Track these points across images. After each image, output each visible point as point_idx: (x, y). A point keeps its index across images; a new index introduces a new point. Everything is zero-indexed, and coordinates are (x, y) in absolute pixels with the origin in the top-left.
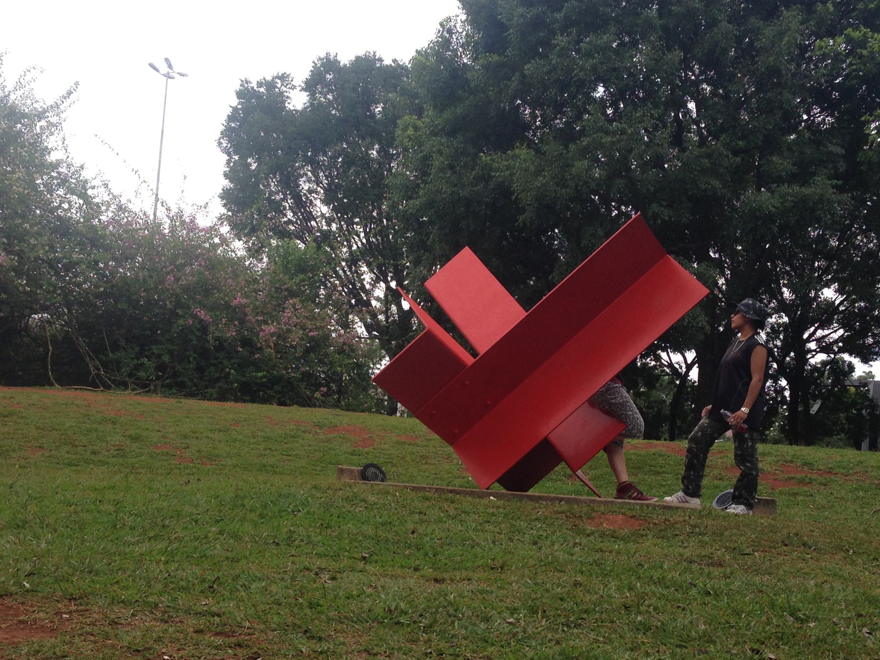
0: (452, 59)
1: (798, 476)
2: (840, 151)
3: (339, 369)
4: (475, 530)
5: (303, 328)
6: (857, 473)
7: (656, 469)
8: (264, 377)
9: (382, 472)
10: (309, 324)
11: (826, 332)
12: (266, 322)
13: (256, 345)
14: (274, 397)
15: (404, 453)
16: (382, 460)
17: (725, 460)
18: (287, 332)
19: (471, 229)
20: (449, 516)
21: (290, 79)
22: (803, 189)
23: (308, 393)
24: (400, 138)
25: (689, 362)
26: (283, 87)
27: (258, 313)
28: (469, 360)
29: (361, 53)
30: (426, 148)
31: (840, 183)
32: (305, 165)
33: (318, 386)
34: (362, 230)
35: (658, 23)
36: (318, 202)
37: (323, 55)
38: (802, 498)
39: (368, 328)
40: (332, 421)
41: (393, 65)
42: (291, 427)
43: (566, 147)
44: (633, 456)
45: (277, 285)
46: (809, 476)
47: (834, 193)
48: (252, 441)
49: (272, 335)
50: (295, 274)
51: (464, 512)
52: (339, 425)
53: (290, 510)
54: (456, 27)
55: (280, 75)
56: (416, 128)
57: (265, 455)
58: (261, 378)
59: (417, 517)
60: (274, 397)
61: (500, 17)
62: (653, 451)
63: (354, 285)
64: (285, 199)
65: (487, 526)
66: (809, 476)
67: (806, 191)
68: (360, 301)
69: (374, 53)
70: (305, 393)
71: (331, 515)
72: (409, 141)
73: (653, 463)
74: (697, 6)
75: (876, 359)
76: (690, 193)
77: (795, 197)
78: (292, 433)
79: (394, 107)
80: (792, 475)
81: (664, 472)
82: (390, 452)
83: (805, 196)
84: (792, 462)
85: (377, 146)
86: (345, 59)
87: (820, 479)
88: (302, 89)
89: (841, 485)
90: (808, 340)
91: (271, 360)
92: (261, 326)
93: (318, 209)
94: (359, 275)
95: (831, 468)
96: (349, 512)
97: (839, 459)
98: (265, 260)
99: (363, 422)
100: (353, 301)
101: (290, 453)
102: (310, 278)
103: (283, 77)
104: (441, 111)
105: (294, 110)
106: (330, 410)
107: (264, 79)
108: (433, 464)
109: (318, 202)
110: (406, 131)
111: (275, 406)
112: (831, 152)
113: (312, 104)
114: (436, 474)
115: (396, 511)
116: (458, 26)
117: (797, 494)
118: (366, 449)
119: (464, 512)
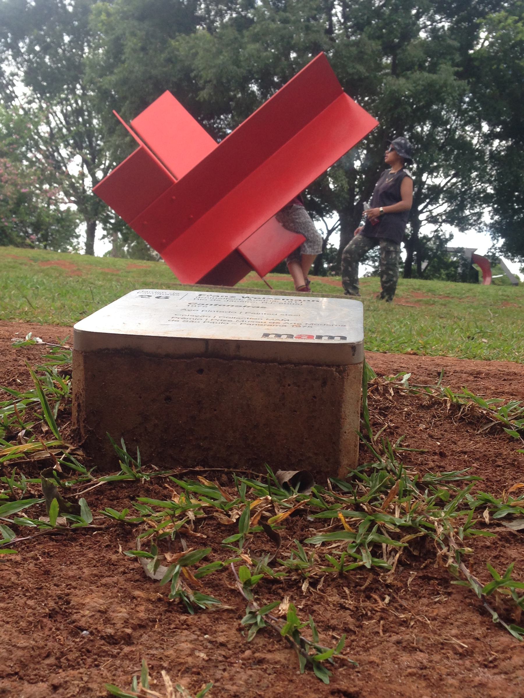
1: (425, 299)
5: (15, 185)
6: (468, 297)
10: (19, 181)
17: (368, 288)
22: (431, 75)
25: (330, 228)
28: (176, 181)
30: (118, 31)
31: (461, 69)
42: (9, 260)
46: (433, 299)
47: (455, 80)
56: (108, 15)
66: (433, 299)
67: (434, 77)
84: (419, 289)
87: (442, 301)
110: (99, 16)
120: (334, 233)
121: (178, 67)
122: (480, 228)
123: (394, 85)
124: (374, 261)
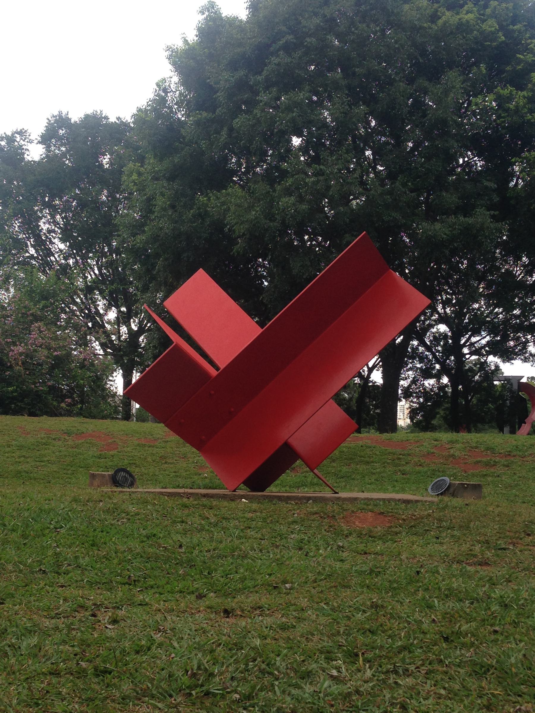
0: (168, 114)
1: (484, 459)
2: (493, 185)
3: (82, 382)
4: (239, 538)
5: (49, 348)
6: (531, 455)
7: (366, 459)
8: (16, 391)
9: (131, 475)
11: (478, 338)
12: (14, 343)
13: (6, 364)
14: (25, 408)
15: (145, 455)
16: (126, 462)
17: (421, 448)
18: (34, 352)
19: (191, 260)
20: (211, 523)
21: (28, 134)
22: (467, 219)
23: (55, 403)
24: (126, 183)
26: (22, 141)
27: (7, 336)
28: (214, 373)
29: (89, 112)
30: (149, 192)
31: (496, 213)
32: (44, 209)
33: (63, 397)
34: (95, 263)
35: (343, 83)
36: (56, 241)
37: (56, 113)
38: (491, 478)
39: (103, 346)
40: (79, 428)
41: (117, 122)
42: (43, 436)
43: (272, 186)
44: (344, 449)
45: (23, 311)
46: (493, 459)
47: (491, 222)
48: (8, 449)
49: (21, 354)
50: (39, 302)
51: (223, 518)
52: (85, 432)
53: (52, 526)
54: (170, 87)
55: (19, 130)
57: (20, 463)
58: (12, 392)
59: (179, 526)
60: (25, 408)
61: (209, 80)
62: (361, 443)
63: (89, 310)
64: (29, 238)
65: (250, 533)
66: (493, 459)
67: (470, 220)
68: (95, 324)
69: (101, 111)
70: (52, 404)
71: (95, 530)
72: (134, 185)
73: (362, 454)
74: (377, 68)
75: (516, 358)
76: (377, 225)
77: (461, 226)
78: (43, 441)
79: (120, 158)
80: (479, 459)
81: (373, 462)
82: (133, 454)
83: (469, 224)
85: (105, 192)
86: (76, 116)
87: (503, 461)
88: (39, 142)
89: (520, 466)
90: (464, 345)
91: (20, 376)
92: (10, 347)
93: (56, 247)
94: (94, 302)
95: (510, 451)
96: (112, 525)
97: (515, 443)
98: (12, 290)
99: (107, 428)
100: (90, 325)
101: (42, 459)
102: (52, 304)
103: (21, 133)
104: (161, 160)
105: (32, 161)
106: (75, 419)
107: (5, 133)
108: (171, 463)
109: (56, 241)
110: (131, 176)
111: (26, 417)
112: (486, 187)
113: (47, 156)
114: (175, 472)
115: (158, 522)
116: (172, 86)
117: (486, 475)
118: (112, 453)
119: (223, 518)
120: (375, 371)
121: (208, 221)
122: (525, 358)
123: (430, 230)
124: (418, 397)
